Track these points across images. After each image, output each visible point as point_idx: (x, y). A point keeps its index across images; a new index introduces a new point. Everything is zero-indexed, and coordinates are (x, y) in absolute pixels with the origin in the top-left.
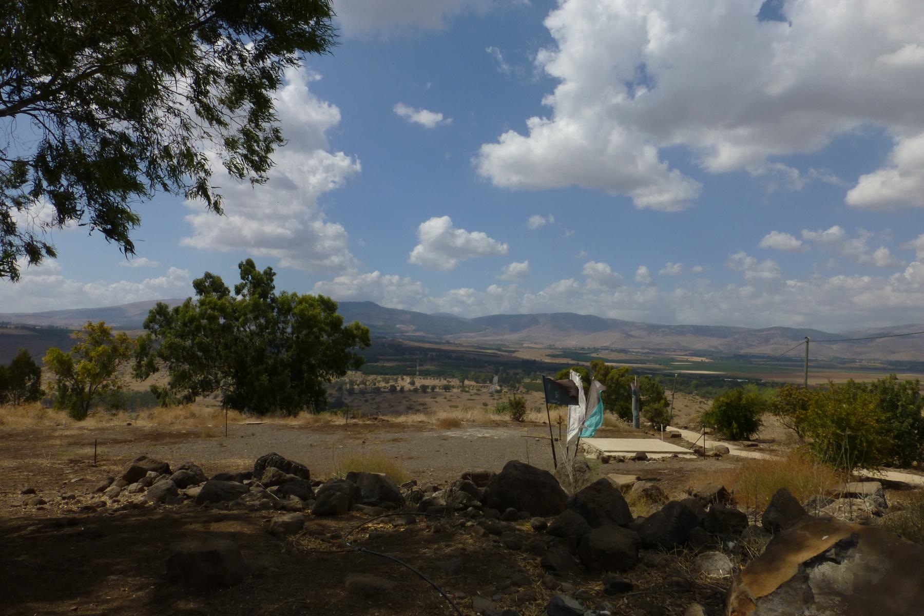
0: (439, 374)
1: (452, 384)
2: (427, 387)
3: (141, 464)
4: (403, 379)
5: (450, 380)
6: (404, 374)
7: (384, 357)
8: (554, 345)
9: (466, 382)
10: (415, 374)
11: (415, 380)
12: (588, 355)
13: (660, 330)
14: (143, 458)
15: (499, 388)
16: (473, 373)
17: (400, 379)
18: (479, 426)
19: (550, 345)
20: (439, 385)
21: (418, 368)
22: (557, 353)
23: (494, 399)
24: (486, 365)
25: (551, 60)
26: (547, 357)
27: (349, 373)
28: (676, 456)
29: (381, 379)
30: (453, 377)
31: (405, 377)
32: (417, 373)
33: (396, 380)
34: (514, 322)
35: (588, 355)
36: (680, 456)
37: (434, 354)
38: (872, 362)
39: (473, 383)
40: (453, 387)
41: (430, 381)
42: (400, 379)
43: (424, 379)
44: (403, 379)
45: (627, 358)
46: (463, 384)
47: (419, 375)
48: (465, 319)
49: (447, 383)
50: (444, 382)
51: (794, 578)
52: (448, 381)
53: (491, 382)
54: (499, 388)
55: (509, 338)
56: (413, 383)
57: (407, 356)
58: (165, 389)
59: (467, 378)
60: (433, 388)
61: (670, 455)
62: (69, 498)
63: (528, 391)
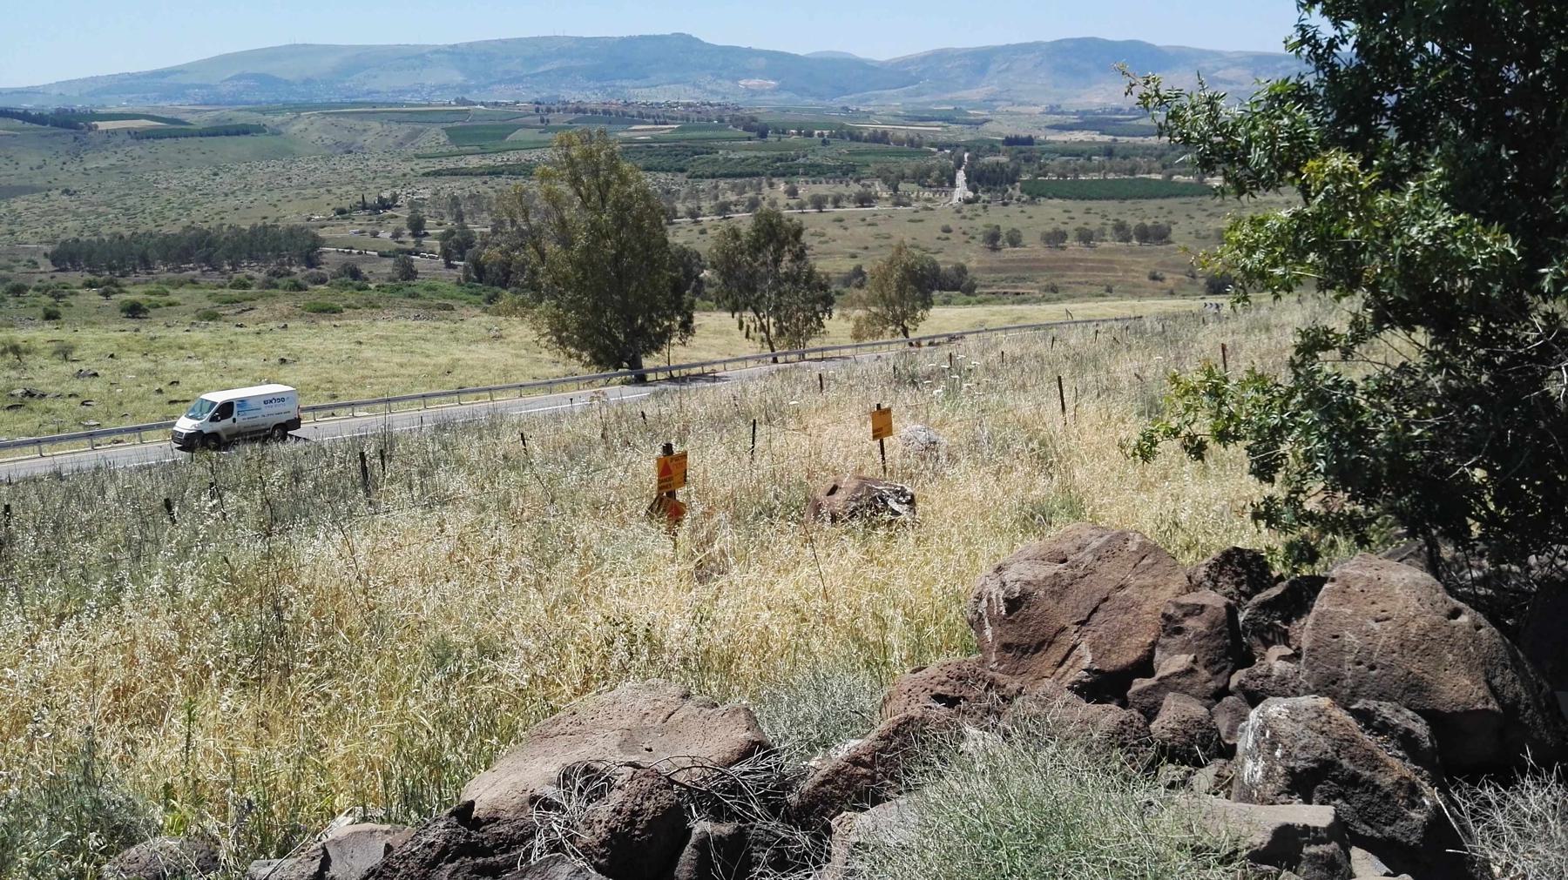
4: (771, 185)
6: (773, 175)
8: (1059, 106)
12: (1135, 122)
13: (1279, 66)
15: (970, 195)
17: (765, 184)
18: (239, 434)
19: (1052, 107)
22: (1069, 121)
26: (1048, 131)
27: (247, 228)
29: (726, 186)
31: (775, 180)
33: (759, 189)
34: (981, 61)
35: (1135, 122)
38: (1034, 247)
42: (765, 184)
43: (814, 183)
44: (771, 185)
47: (806, 174)
49: (862, 190)
50: (855, 188)
51: (1334, 696)
52: (863, 186)
54: (970, 195)
55: (972, 95)
56: (793, 193)
63: (1033, 198)
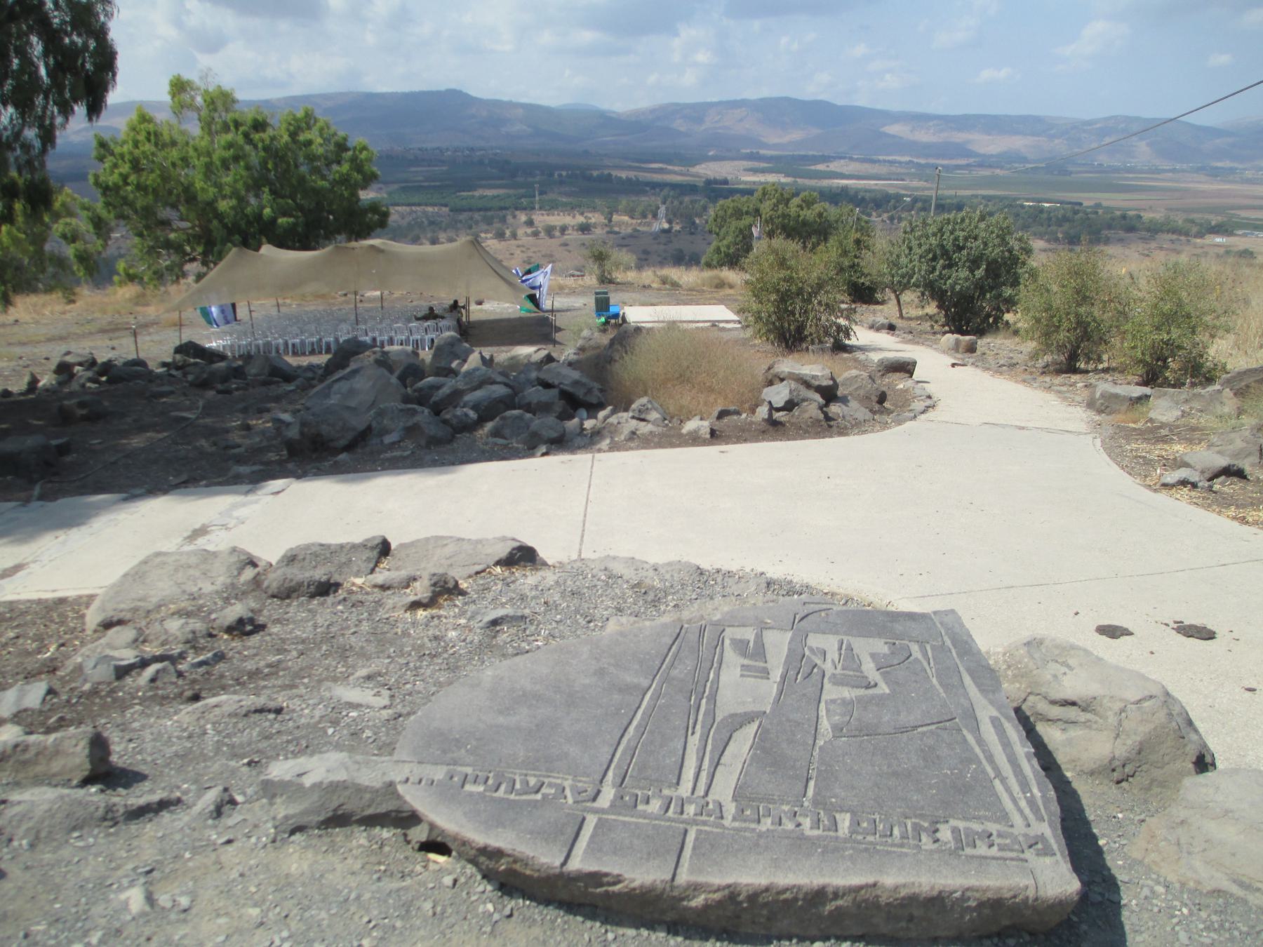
0: (571, 208)
1: (593, 220)
2: (553, 228)
3: (69, 359)
5: (590, 215)
7: (484, 182)
9: (615, 218)
10: (533, 208)
11: (534, 217)
14: (68, 353)
16: (624, 202)
20: (572, 224)
21: (537, 198)
23: (659, 243)
24: (648, 189)
25: (159, 106)
28: (714, 325)
30: (594, 209)
31: (517, 213)
32: (537, 206)
36: (721, 325)
37: (564, 173)
39: (626, 218)
40: (595, 226)
41: (558, 218)
44: (514, 217)
45: (875, 171)
46: (610, 221)
47: (541, 208)
48: (614, 112)
49: (584, 221)
50: (580, 219)
53: (655, 216)
54: (666, 226)
57: (520, 179)
58: (115, 184)
59: (617, 211)
60: (563, 229)
61: (709, 324)
62: (462, 210)
